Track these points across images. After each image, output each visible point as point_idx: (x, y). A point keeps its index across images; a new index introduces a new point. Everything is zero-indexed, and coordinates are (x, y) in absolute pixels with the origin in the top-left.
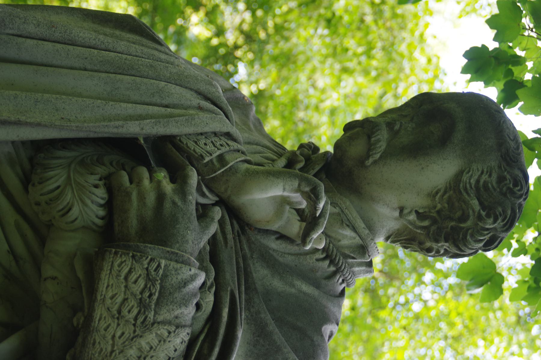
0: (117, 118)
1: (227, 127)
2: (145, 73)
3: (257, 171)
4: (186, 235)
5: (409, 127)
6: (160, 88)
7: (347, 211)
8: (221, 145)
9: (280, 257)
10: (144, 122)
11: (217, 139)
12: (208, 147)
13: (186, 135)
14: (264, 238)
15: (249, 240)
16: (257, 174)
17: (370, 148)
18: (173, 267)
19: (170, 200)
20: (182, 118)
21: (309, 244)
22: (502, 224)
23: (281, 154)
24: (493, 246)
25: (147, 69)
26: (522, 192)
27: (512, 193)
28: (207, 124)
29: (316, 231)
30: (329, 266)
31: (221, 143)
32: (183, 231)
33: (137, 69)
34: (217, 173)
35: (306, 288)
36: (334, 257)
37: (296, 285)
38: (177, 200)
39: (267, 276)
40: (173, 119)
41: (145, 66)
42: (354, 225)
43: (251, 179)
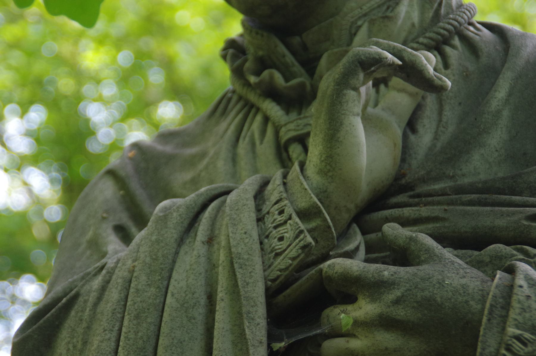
1: (247, 200)
2: (152, 329)
3: (327, 157)
4: (454, 288)
6: (179, 306)
8: (281, 212)
9: (447, 129)
10: (250, 338)
11: (268, 218)
12: (286, 234)
13: (265, 271)
14: (415, 154)
15: (424, 181)
16: (332, 158)
18: (520, 314)
19: (392, 308)
20: (238, 274)
21: (445, 82)
23: (246, 109)
25: (144, 325)
28: (245, 233)
30: (453, 47)
31: (277, 212)
32: (447, 291)
33: (143, 341)
34: (331, 224)
36: (439, 37)
37: (498, 107)
38: (391, 296)
39: (483, 154)
40: (241, 290)
41: (137, 328)
43: (340, 169)
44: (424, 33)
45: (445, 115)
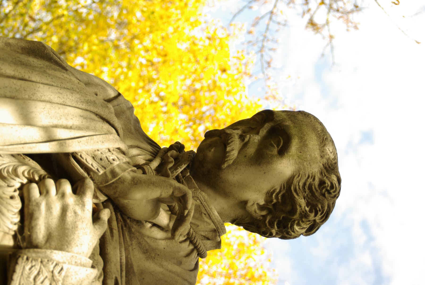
5: (255, 139)
7: (205, 203)
8: (114, 160)
19: (72, 210)
22: (320, 216)
24: (312, 232)
26: (336, 193)
29: (183, 226)
30: (189, 245)
42: (209, 214)
44: (194, 231)
45: (159, 241)
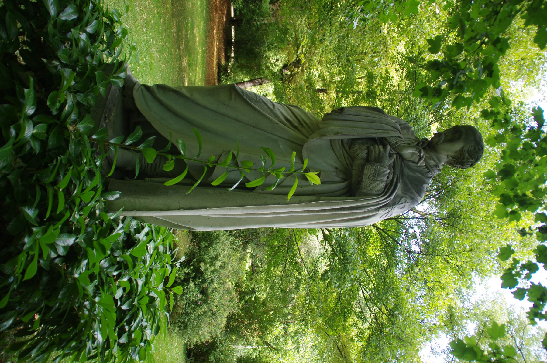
0: (371, 133)
15: (404, 163)
17: (439, 140)
27: (477, 152)
35: (419, 175)
